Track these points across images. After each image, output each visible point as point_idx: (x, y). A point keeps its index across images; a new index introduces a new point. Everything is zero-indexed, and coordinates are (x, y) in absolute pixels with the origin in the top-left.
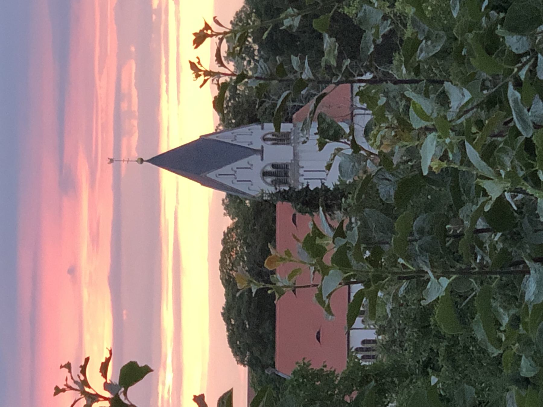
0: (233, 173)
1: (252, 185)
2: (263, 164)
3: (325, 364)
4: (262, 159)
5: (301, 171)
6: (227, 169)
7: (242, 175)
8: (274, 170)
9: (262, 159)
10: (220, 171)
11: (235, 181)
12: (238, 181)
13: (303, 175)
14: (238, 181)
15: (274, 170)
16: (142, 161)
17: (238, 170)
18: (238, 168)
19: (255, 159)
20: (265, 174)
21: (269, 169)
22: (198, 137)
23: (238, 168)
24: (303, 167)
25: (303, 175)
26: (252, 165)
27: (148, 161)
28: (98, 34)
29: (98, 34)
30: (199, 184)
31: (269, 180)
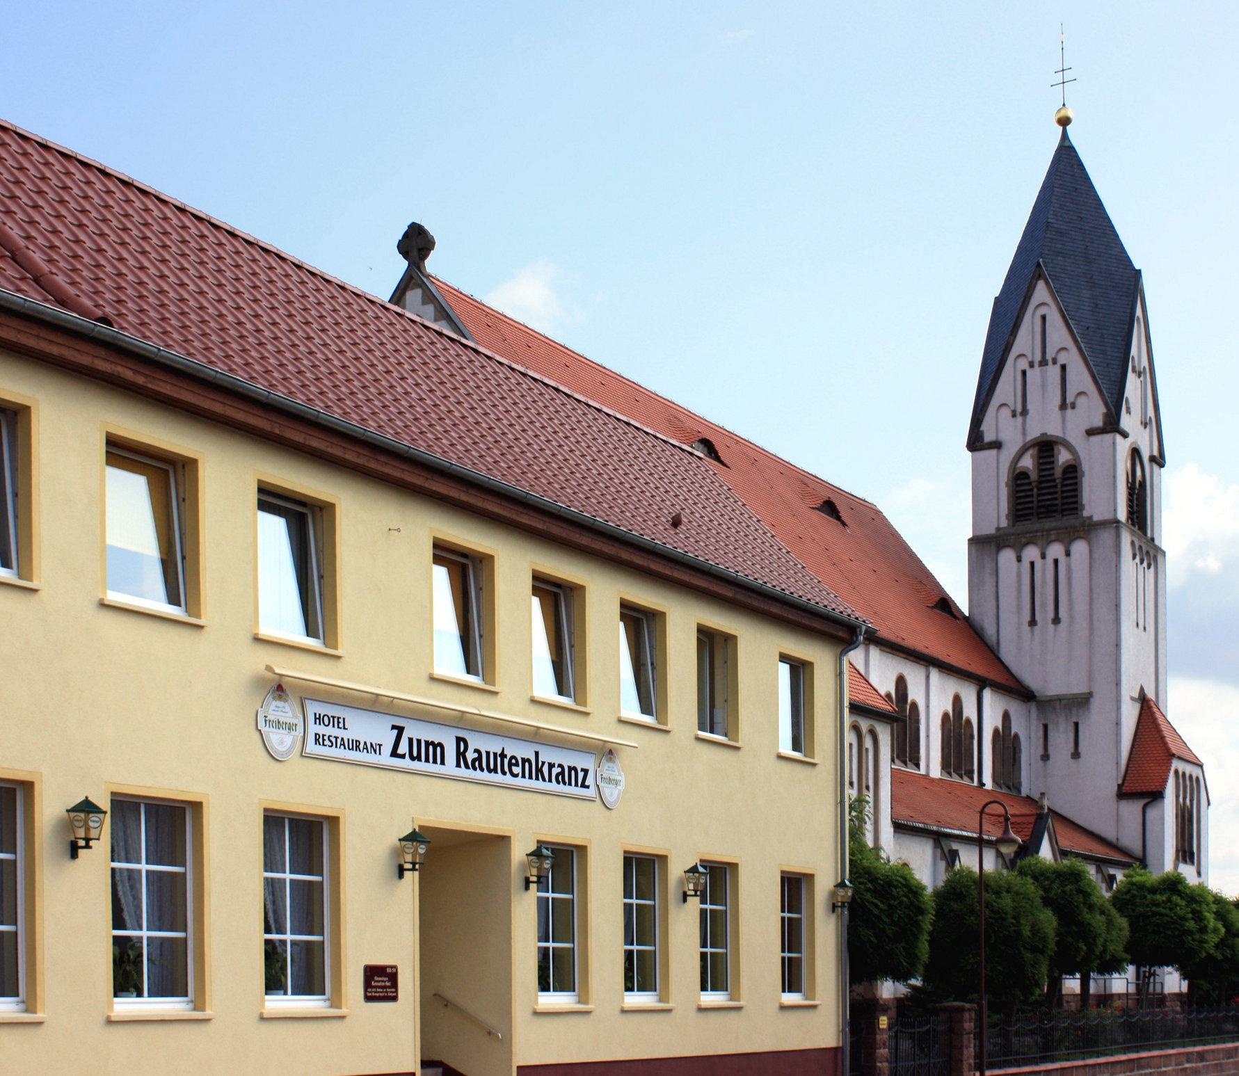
0: (1049, 357)
1: (1014, 415)
2: (1074, 435)
3: (1063, 113)
4: (1091, 432)
5: (1056, 550)
6: (1059, 335)
7: (1044, 384)
8: (1058, 473)
9: (1091, 432)
10: (1055, 319)
11: (1023, 364)
12: (1024, 373)
13: (1043, 556)
14: (1024, 373)
15: (1058, 473)
16: (1064, 122)
17: (1057, 369)
18: (1063, 367)
19: (1092, 410)
20: (1045, 447)
21: (1063, 457)
22: (1137, 267)
23: (1063, 367)
24: (1068, 554)
25: (1043, 556)
26: (1073, 406)
27: (1065, 136)
28: (1102, 1060)
29: (1102, 1060)
30: (997, 292)
31: (1027, 462)
